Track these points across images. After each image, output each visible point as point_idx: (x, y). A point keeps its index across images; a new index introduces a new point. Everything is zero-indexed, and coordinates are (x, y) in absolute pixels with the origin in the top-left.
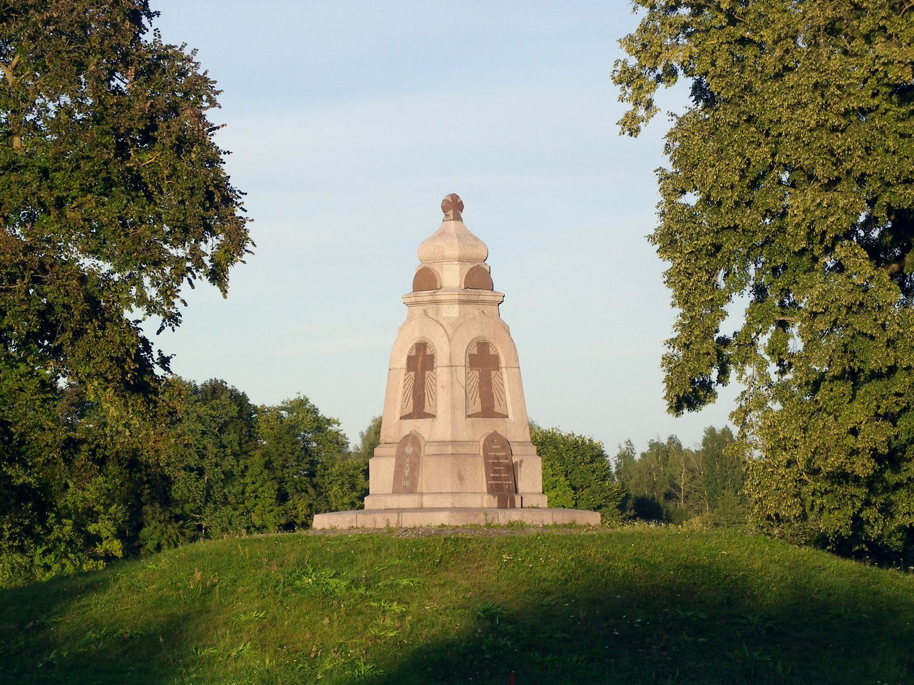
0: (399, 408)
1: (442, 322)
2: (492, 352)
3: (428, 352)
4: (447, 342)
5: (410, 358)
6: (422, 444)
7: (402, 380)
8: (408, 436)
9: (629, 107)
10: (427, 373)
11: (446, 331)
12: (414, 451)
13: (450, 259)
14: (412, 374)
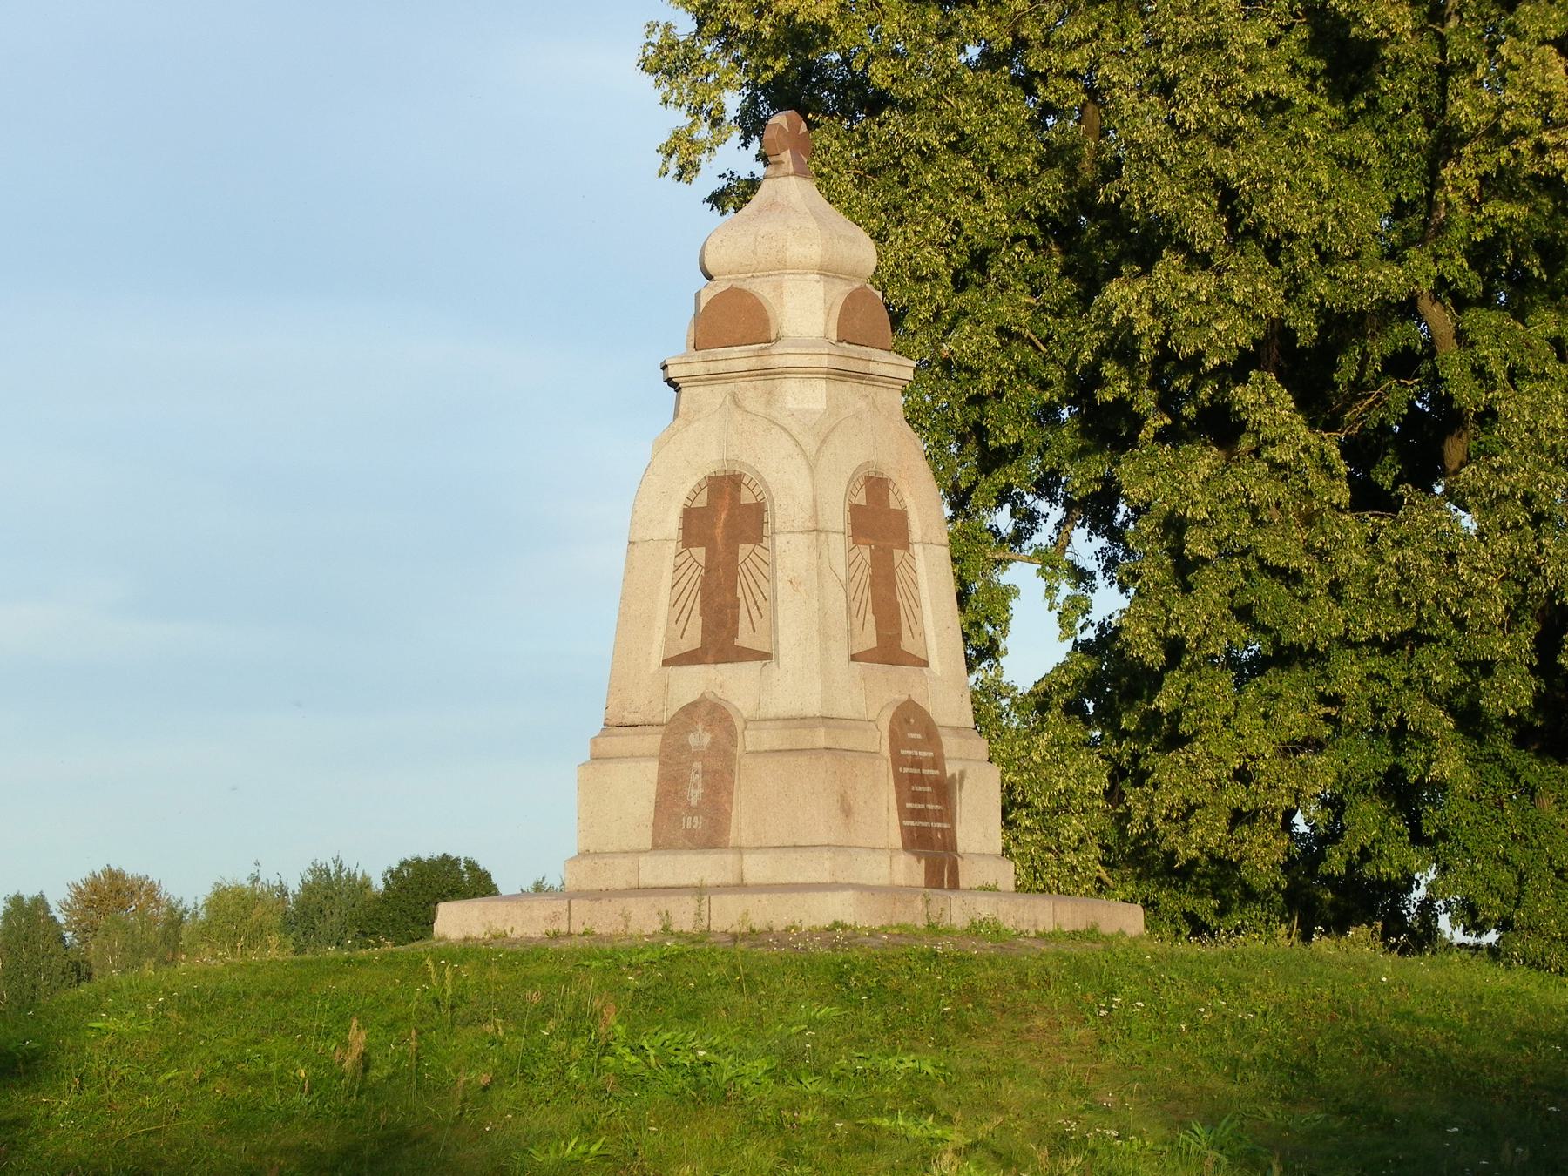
0: (659, 638)
1: (786, 422)
2: (894, 504)
3: (747, 497)
4: (805, 471)
5: (689, 515)
6: (739, 724)
7: (669, 571)
8: (694, 704)
9: (680, 118)
10: (744, 550)
11: (798, 444)
12: (713, 743)
13: (800, 269)
14: (700, 553)
